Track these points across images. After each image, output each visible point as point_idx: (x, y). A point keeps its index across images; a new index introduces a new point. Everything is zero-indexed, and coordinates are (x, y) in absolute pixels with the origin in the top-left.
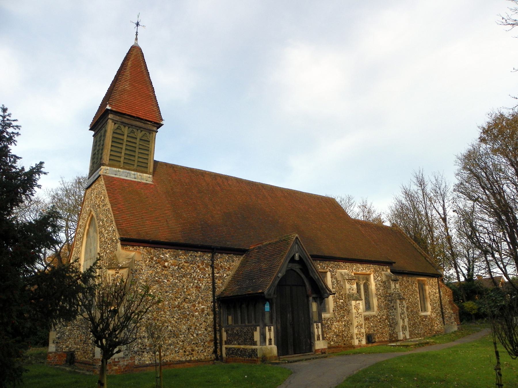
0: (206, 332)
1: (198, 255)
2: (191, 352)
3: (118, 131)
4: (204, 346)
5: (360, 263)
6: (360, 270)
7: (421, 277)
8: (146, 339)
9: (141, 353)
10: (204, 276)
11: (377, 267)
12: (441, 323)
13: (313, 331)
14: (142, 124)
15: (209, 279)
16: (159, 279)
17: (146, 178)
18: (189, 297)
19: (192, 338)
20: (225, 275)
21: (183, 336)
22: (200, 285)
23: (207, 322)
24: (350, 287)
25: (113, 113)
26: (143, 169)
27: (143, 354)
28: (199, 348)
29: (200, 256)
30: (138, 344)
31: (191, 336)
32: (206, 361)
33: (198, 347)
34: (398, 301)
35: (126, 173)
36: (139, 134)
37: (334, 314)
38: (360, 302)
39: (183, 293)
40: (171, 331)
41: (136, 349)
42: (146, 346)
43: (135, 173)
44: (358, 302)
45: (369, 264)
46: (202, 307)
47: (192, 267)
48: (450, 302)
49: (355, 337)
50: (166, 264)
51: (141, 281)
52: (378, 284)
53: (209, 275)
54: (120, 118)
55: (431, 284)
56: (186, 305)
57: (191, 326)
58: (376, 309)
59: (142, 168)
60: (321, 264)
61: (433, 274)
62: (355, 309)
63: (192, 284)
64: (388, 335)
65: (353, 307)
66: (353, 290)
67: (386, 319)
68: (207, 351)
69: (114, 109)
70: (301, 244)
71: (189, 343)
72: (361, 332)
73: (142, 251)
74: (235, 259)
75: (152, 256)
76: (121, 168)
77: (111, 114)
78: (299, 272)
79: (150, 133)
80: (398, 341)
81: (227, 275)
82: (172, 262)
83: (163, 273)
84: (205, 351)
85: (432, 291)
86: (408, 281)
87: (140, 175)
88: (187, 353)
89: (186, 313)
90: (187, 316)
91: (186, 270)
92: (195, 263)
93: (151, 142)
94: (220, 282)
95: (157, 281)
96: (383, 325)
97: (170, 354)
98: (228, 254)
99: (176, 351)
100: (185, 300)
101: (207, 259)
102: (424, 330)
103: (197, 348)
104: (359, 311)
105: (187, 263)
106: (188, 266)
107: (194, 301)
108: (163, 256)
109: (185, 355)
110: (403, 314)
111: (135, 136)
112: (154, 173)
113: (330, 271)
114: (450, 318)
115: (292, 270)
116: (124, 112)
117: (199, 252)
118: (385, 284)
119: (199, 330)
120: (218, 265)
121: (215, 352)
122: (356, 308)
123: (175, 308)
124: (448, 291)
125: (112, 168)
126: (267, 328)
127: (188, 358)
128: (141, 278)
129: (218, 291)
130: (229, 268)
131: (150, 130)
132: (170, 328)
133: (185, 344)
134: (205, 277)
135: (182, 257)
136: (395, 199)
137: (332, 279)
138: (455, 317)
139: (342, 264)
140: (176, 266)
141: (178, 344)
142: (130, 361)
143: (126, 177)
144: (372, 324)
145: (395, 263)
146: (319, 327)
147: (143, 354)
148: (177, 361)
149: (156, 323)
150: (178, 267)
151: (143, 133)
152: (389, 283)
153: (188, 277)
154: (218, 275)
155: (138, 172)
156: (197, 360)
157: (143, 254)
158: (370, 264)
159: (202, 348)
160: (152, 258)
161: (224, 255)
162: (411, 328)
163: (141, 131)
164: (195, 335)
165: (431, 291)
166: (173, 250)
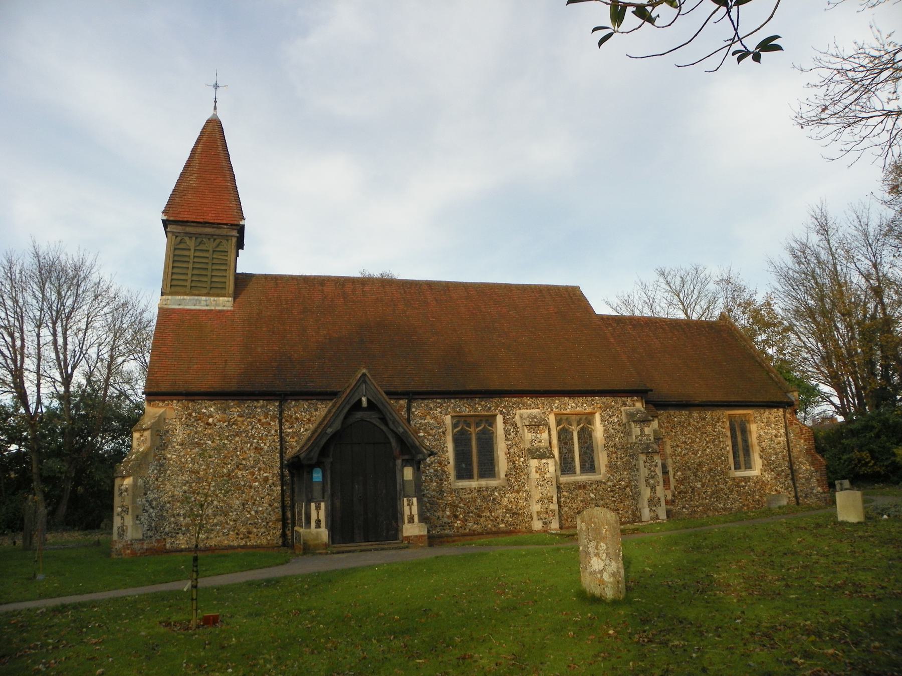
0: (270, 509)
1: (259, 405)
2: (247, 535)
3: (181, 246)
4: (266, 527)
5: (570, 397)
6: (570, 407)
7: (737, 410)
8: (182, 517)
9: (174, 535)
10: (268, 433)
11: (609, 400)
12: (790, 489)
13: (401, 509)
14: (215, 229)
15: (276, 437)
16: (200, 440)
17: (224, 303)
18: (244, 462)
19: (248, 516)
20: (302, 430)
21: (235, 513)
22: (262, 445)
23: (272, 496)
24: (533, 438)
25: (171, 223)
26: (219, 291)
27: (177, 536)
28: (259, 530)
29: (262, 407)
30: (170, 523)
31: (246, 513)
32: (267, 548)
33: (257, 528)
34: (643, 457)
35: (194, 301)
36: (210, 245)
37: (508, 480)
38: (551, 462)
39: (235, 457)
40: (217, 508)
41: (167, 529)
42: (181, 525)
43: (207, 298)
44: (544, 461)
45: (591, 397)
46: (265, 475)
47: (249, 422)
48: (808, 451)
49: (535, 517)
50: (211, 420)
51: (175, 444)
52: (610, 429)
53: (276, 431)
54: (183, 227)
55: (765, 420)
56: (239, 473)
57: (247, 501)
58: (603, 469)
59: (215, 290)
60: (483, 403)
61: (768, 402)
62: (537, 472)
63: (249, 445)
64: (630, 512)
65: (534, 470)
66: (540, 442)
67: (627, 486)
68: (271, 533)
69: (171, 218)
70: (372, 383)
71: (244, 523)
72: (549, 509)
73: (176, 406)
74: (319, 406)
75: (189, 411)
76: (187, 295)
77: (170, 224)
78: (378, 424)
79: (227, 240)
80: (642, 522)
81: (306, 430)
82: (218, 417)
83: (206, 432)
84: (269, 534)
85: (766, 433)
86: (704, 419)
87: (214, 300)
88: (242, 536)
89: (240, 484)
90: (241, 488)
91: (240, 427)
92: (254, 417)
93: (229, 253)
94: (294, 440)
95: (197, 443)
96: (619, 496)
97: (216, 537)
98: (307, 400)
99: (224, 533)
100: (238, 466)
101: (273, 409)
102: (741, 502)
103: (255, 530)
104: (546, 476)
105: (241, 417)
106: (243, 421)
107: (252, 467)
108: (205, 411)
109: (238, 538)
110: (653, 477)
111: (207, 249)
112: (236, 296)
113: (501, 414)
114: (808, 480)
115: (363, 420)
116: (186, 219)
117: (261, 401)
118: (625, 428)
119: (259, 505)
120: (292, 417)
121: (284, 535)
122: (539, 471)
123: (223, 477)
124: (804, 431)
125: (174, 297)
126: (313, 505)
127: (243, 543)
128: (175, 440)
129: (290, 453)
130: (309, 420)
131: (227, 236)
132: (215, 503)
133: (238, 524)
134: (269, 434)
135: (234, 409)
136: (770, 264)
137: (506, 426)
138: (819, 478)
139: (528, 400)
140: (225, 422)
141: (228, 524)
142: (156, 544)
143: (195, 305)
144: (592, 495)
145: (651, 390)
146: (412, 504)
147: (177, 536)
148: (226, 546)
149: (195, 498)
150: (229, 424)
151: (218, 241)
152: (630, 425)
153: (244, 435)
154: (291, 430)
155: (211, 296)
156: (255, 545)
157: (177, 410)
158: (594, 397)
159: (263, 530)
160: (190, 415)
161: (302, 402)
162: (706, 499)
163: (215, 240)
164: (253, 513)
165: (764, 432)
166: (219, 401)
